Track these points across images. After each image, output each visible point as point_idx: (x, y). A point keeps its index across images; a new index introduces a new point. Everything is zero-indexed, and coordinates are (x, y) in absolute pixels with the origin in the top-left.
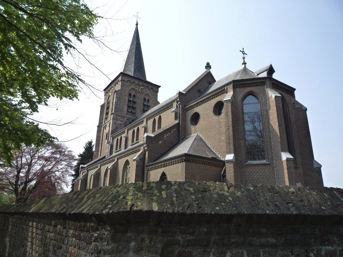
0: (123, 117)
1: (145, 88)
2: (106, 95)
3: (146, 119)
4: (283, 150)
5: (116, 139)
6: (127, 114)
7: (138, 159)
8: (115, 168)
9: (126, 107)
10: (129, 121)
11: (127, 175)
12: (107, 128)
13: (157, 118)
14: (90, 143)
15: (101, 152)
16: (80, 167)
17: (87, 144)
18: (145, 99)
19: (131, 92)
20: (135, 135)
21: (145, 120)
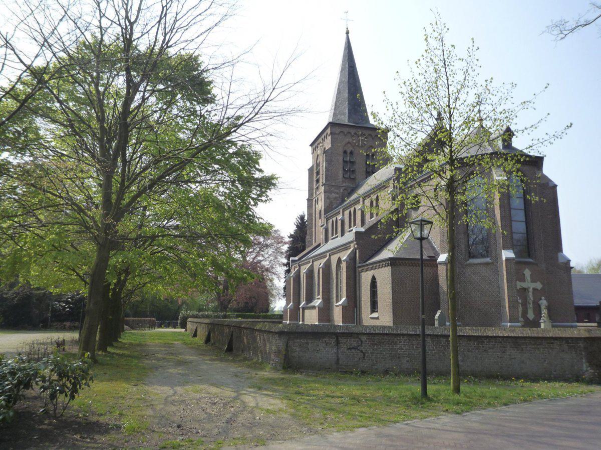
0: (338, 187)
4: (505, 248)
6: (343, 182)
7: (348, 260)
8: (328, 266)
10: (347, 191)
12: (320, 203)
14: (302, 218)
15: (315, 236)
16: (291, 260)
17: (298, 219)
19: (346, 148)
20: (352, 217)
21: (361, 199)
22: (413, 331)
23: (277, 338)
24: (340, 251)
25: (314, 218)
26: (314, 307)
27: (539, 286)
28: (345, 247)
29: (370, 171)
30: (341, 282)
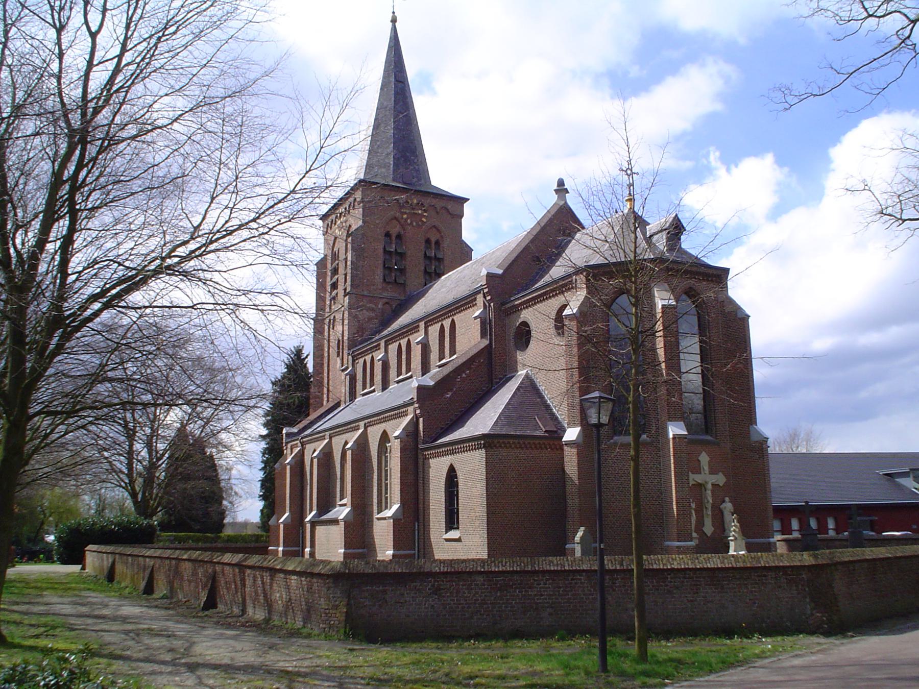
1: (425, 211)
2: (327, 232)
3: (425, 323)
5: (361, 361)
6: (384, 289)
7: (404, 436)
8: (362, 445)
9: (380, 272)
11: (386, 462)
12: (339, 328)
13: (447, 323)
16: (284, 431)
18: (428, 241)
20: (404, 357)
21: (422, 325)
22: (557, 565)
23: (331, 585)
24: (385, 420)
25: (326, 355)
26: (335, 522)
27: (720, 479)
28: (396, 412)
29: (433, 274)
30: (386, 475)
